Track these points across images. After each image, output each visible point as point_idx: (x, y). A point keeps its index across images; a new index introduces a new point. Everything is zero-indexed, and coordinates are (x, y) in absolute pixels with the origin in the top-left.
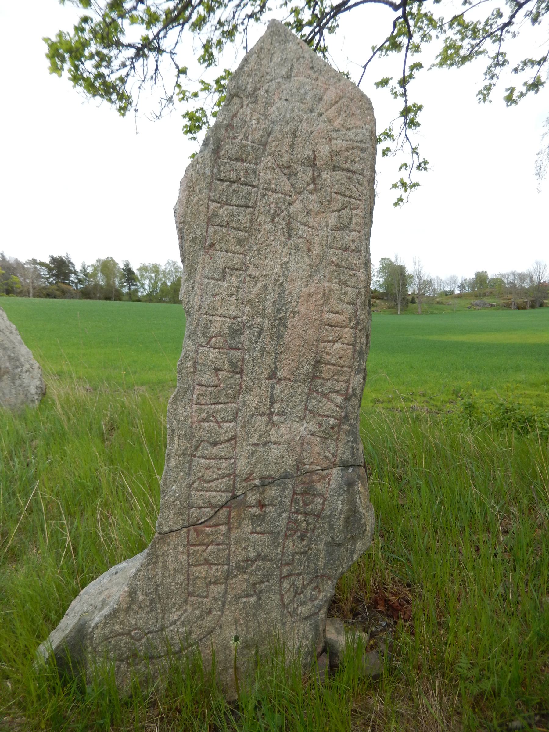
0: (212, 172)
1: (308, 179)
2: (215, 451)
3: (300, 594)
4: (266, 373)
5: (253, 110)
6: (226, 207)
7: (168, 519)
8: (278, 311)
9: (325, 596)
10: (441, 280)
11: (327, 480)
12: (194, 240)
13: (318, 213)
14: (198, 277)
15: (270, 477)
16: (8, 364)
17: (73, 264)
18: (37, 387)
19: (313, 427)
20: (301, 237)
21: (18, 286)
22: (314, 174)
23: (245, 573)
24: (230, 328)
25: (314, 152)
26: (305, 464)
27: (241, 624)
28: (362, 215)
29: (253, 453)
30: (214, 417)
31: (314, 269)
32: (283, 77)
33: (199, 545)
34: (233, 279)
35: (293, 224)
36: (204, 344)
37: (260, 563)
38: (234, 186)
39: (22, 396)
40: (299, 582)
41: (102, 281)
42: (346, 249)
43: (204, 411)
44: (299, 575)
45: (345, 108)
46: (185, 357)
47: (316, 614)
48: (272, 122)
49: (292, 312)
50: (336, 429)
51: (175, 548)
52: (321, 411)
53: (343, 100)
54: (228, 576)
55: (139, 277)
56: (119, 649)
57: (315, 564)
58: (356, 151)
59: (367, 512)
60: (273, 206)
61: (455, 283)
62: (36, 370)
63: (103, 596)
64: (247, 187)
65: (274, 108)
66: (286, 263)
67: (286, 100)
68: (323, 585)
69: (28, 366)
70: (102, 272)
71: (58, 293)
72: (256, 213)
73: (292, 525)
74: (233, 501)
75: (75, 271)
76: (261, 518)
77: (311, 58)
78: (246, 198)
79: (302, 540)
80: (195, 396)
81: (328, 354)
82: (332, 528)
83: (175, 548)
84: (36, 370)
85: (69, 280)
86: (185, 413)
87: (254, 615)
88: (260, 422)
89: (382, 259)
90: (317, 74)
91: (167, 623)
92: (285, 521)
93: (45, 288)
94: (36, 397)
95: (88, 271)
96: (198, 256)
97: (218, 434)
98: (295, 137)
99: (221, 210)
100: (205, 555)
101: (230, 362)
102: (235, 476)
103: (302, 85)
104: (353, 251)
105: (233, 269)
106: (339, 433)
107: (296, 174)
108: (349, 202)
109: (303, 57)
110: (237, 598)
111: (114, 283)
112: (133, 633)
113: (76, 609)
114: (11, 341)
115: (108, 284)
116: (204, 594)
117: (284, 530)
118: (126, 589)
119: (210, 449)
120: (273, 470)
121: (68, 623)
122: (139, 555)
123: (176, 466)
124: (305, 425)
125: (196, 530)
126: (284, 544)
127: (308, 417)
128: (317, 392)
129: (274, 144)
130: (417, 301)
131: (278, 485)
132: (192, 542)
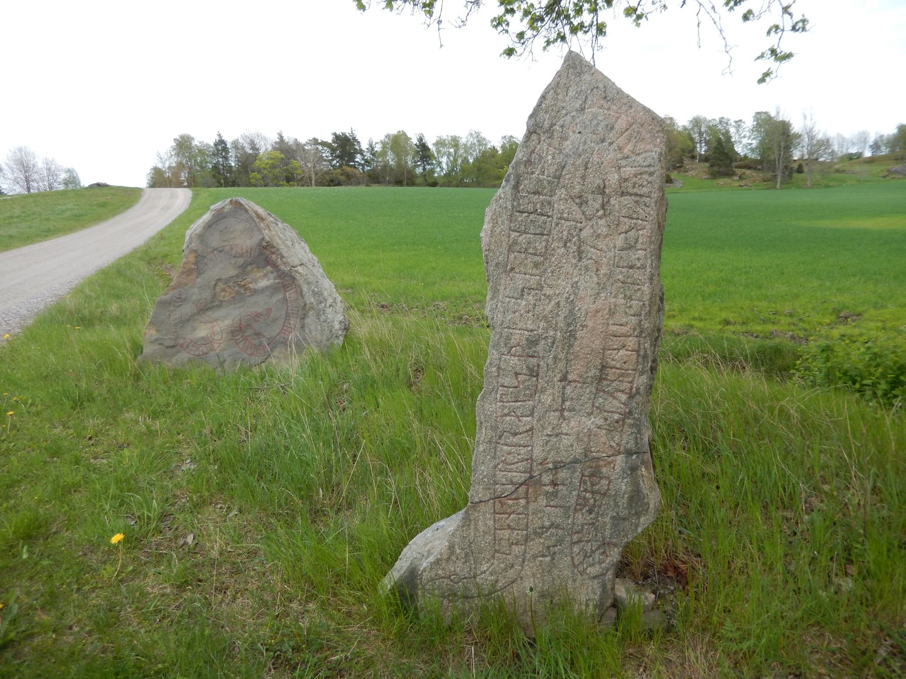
0: (513, 205)
2: (515, 440)
4: (559, 376)
5: (550, 145)
6: (524, 236)
8: (569, 325)
10: (843, 139)
12: (497, 264)
13: (606, 236)
14: (500, 297)
15: (562, 462)
17: (359, 142)
18: (340, 322)
19: (600, 422)
21: (298, 172)
24: (527, 339)
25: (604, 181)
31: (602, 287)
32: (577, 110)
34: (530, 297)
38: (532, 216)
42: (631, 267)
44: (588, 541)
47: (604, 574)
48: (566, 156)
50: (621, 423)
51: (484, 514)
52: (607, 408)
54: (527, 539)
55: (436, 155)
58: (643, 176)
59: (651, 492)
60: (565, 233)
61: (865, 141)
65: (568, 142)
66: (577, 282)
67: (580, 133)
70: (391, 149)
75: (361, 150)
76: (554, 495)
79: (591, 513)
82: (616, 505)
83: (484, 514)
84: (339, 304)
85: (354, 161)
87: (549, 571)
88: (553, 417)
89: (758, 113)
91: (478, 572)
92: (575, 498)
93: (327, 173)
94: (340, 333)
97: (517, 426)
99: (520, 238)
100: (508, 521)
101: (528, 367)
103: (595, 116)
104: (638, 268)
106: (623, 425)
107: (587, 202)
108: (636, 224)
110: (535, 557)
113: (408, 555)
114: (314, 275)
115: (399, 164)
119: (511, 438)
120: (563, 457)
122: (454, 516)
123: (484, 451)
125: (500, 502)
129: (567, 176)
130: (805, 169)
131: (568, 469)
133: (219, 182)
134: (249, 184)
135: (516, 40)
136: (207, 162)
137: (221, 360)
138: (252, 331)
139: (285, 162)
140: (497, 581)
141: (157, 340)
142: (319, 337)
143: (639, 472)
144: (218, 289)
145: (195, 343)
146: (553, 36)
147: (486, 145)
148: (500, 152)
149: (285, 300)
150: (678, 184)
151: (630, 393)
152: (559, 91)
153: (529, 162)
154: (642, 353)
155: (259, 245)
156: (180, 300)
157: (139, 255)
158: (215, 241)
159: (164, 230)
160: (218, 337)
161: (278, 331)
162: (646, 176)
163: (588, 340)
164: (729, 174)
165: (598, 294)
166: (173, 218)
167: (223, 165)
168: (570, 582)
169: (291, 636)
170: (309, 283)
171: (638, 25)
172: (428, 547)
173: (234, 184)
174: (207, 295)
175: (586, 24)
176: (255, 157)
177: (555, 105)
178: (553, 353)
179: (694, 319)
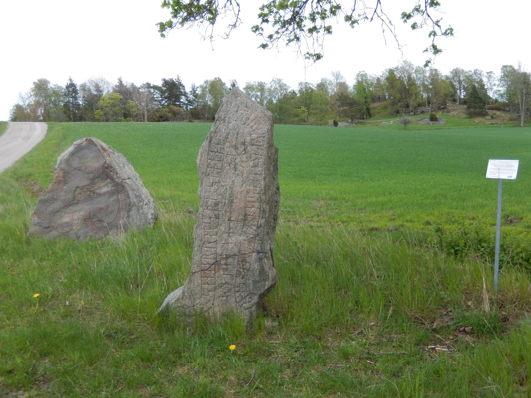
2: (210, 245)
13: (246, 162)
16: (135, 200)
17: (183, 86)
21: (134, 110)
31: (244, 182)
38: (216, 154)
39: (143, 220)
40: (243, 294)
41: (211, 101)
42: (256, 174)
44: (243, 292)
54: (215, 289)
62: (152, 203)
69: (147, 201)
70: (210, 93)
75: (185, 92)
76: (226, 269)
79: (243, 279)
84: (152, 203)
89: (504, 67)
93: (157, 111)
94: (152, 221)
95: (197, 92)
97: (210, 239)
103: (242, 114)
110: (219, 297)
114: (136, 185)
120: (229, 252)
121: (164, 304)
133: (69, 117)
134: (94, 120)
135: (268, 39)
136: (59, 101)
137: (78, 236)
138: (97, 219)
139: (123, 102)
140: (203, 308)
141: (38, 223)
142: (138, 223)
143: (263, 261)
144: (77, 193)
145: (61, 226)
147: (286, 89)
148: (298, 95)
149: (118, 200)
150: (442, 122)
153: (215, 132)
154: (262, 209)
155: (103, 166)
156: (53, 199)
158: (76, 163)
162: (262, 138)
163: (238, 204)
164: (483, 114)
166: (33, 146)
168: (235, 310)
170: (133, 190)
171: (353, 27)
173: (81, 119)
174: (70, 196)
175: (318, 27)
179: (407, 221)
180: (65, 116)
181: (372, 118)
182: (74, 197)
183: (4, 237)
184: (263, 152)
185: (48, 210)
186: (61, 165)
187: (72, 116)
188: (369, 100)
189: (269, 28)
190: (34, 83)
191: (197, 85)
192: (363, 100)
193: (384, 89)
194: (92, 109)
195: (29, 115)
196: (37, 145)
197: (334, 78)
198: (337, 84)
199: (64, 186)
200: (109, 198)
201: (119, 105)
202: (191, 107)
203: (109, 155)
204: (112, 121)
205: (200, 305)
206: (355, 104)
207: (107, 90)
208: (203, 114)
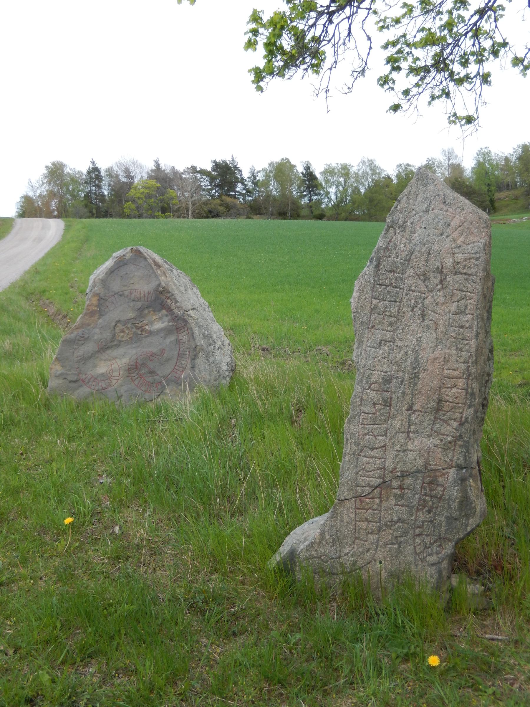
0: (374, 280)
1: (437, 282)
2: (373, 453)
3: (428, 548)
4: (406, 407)
6: (382, 302)
7: (344, 492)
8: (414, 369)
9: (447, 552)
11: (446, 476)
12: (362, 323)
13: (443, 304)
15: (407, 471)
17: (240, 171)
19: (437, 442)
20: (431, 320)
21: (174, 202)
22: (441, 278)
23: (390, 529)
24: (383, 378)
25: (442, 263)
26: (430, 465)
27: (388, 561)
28: (475, 303)
29: (396, 456)
30: (372, 432)
31: (438, 340)
32: (423, 212)
33: (362, 509)
34: (386, 348)
35: (426, 312)
36: (367, 388)
37: (400, 524)
38: (388, 288)
42: (462, 327)
43: (366, 428)
44: (428, 535)
45: (466, 230)
46: (356, 396)
48: (415, 245)
49: (423, 369)
50: (453, 443)
51: (348, 509)
52: (442, 432)
53: (465, 224)
54: (380, 530)
56: (314, 566)
57: (438, 529)
58: (472, 260)
60: (413, 301)
63: (305, 535)
64: (397, 289)
65: (416, 235)
66: (420, 337)
67: (425, 228)
68: (445, 545)
69: (220, 343)
70: (275, 178)
71: (221, 209)
72: (402, 306)
73: (422, 503)
74: (383, 484)
75: (242, 179)
76: (402, 496)
77: (444, 195)
78: (395, 296)
79: (429, 513)
80: (361, 419)
81: (447, 395)
82: (450, 507)
83: (348, 509)
84: (227, 347)
86: (355, 430)
87: (396, 556)
88: (401, 437)
90: (447, 206)
91: (342, 554)
93: (205, 203)
94: (227, 374)
95: (258, 178)
96: (364, 333)
97: (375, 443)
98: (429, 254)
99: (380, 304)
100: (365, 515)
101: (383, 399)
102: (385, 469)
103: (436, 216)
104: (467, 328)
105: (386, 341)
106: (455, 446)
107: (429, 279)
108: (465, 295)
109: (439, 195)
110: (386, 544)
111: (291, 192)
112: (322, 558)
114: (205, 319)
115: (283, 195)
116: (365, 539)
117: (417, 505)
118: (319, 531)
119: (369, 452)
120: (409, 467)
121: (285, 549)
123: (349, 461)
124: (431, 440)
125: (360, 500)
126: (416, 514)
127: (433, 435)
128: (440, 419)
131: (412, 477)
132: (358, 507)
133: (91, 212)
134: (123, 215)
135: (402, 97)
136: (79, 191)
137: (119, 395)
138: (147, 370)
140: (356, 562)
141: (62, 374)
142: (208, 377)
143: (467, 483)
144: (117, 330)
145: (95, 379)
146: (437, 93)
147: (379, 174)
149: (178, 341)
151: (461, 421)
152: (411, 197)
153: (387, 249)
155: (156, 290)
156: (83, 339)
157: (17, 290)
158: (116, 286)
159: (38, 263)
160: (116, 374)
161: (170, 370)
162: (473, 261)
163: (428, 381)
165: (436, 346)
167: (95, 194)
168: (413, 566)
169: (200, 592)
170: (200, 327)
171: (525, 75)
172: (304, 535)
173: (106, 214)
174: (107, 335)
175: (472, 76)
176: (129, 185)
177: (407, 207)
178: (402, 389)
180: (86, 210)
181: (497, 214)
182: (114, 336)
183: (14, 396)
184: (476, 287)
185: (75, 355)
186: (94, 287)
187: (94, 211)
188: (493, 188)
189: (403, 80)
190: (46, 167)
191: (258, 168)
192: (485, 188)
193: (514, 173)
194: (120, 202)
195: (41, 209)
196: (51, 249)
197: (445, 158)
198: (449, 166)
199: (99, 319)
200: (165, 338)
201: (155, 196)
202: (250, 198)
203: (164, 273)
204: (146, 217)
205: (352, 556)
206: (474, 193)
207: (140, 176)
208: (265, 208)
